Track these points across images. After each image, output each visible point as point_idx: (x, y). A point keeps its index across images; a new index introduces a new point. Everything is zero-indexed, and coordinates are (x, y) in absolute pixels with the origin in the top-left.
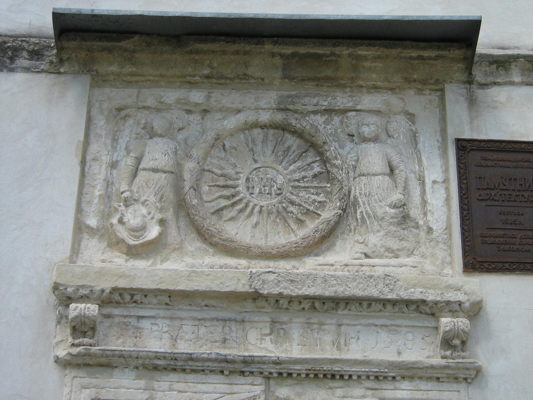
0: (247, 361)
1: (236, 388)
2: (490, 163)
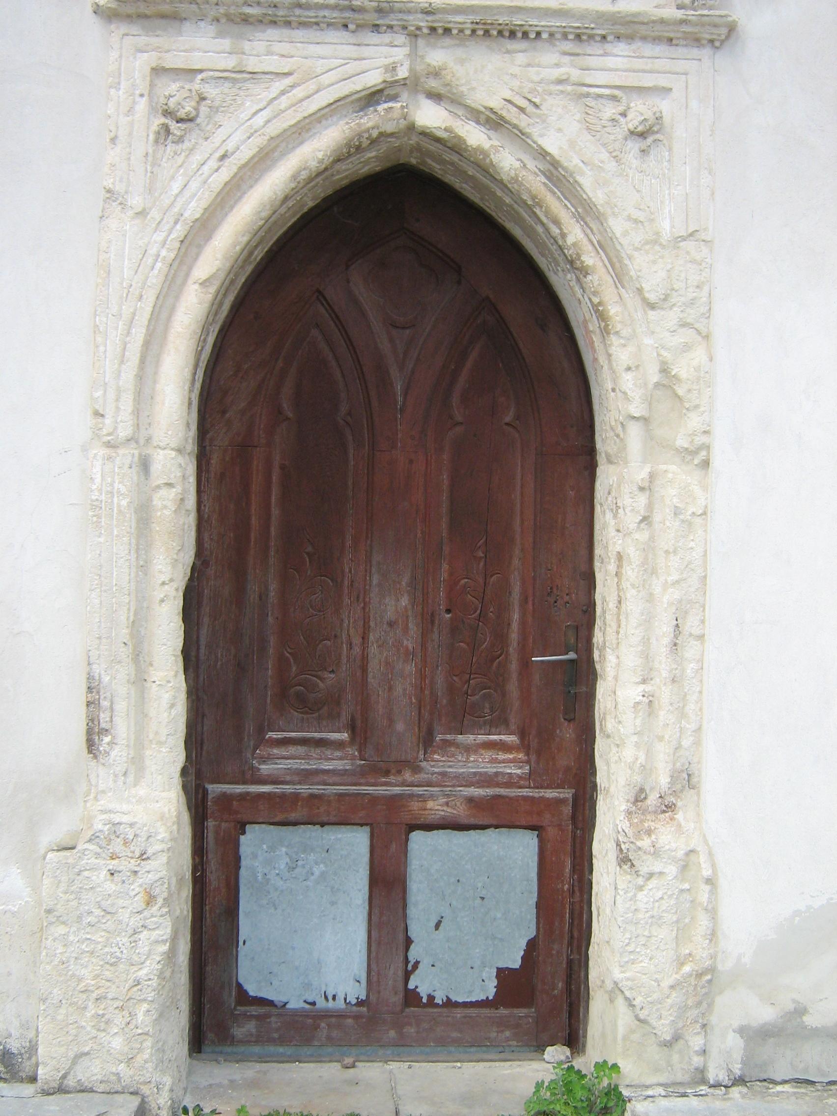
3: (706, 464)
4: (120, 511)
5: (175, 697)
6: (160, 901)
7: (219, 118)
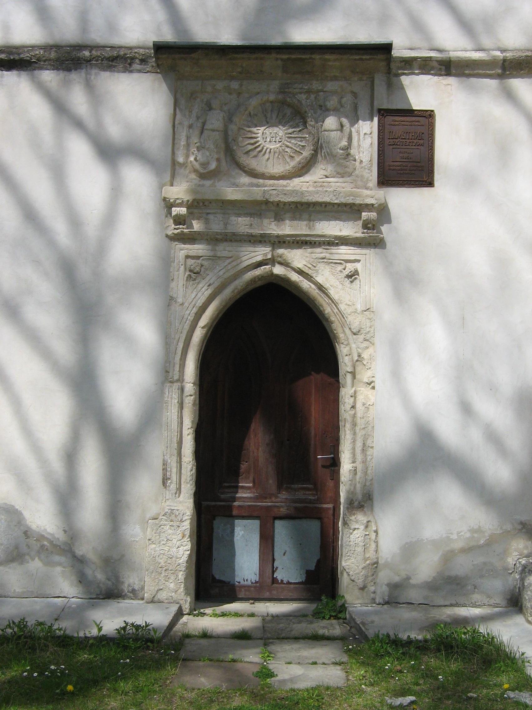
0: (263, 236)
1: (257, 249)
2: (397, 123)
3: (373, 388)
4: (174, 404)
5: (192, 468)
6: (187, 536)
7: (207, 272)
